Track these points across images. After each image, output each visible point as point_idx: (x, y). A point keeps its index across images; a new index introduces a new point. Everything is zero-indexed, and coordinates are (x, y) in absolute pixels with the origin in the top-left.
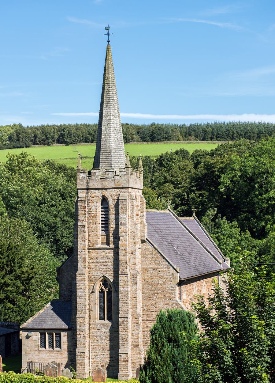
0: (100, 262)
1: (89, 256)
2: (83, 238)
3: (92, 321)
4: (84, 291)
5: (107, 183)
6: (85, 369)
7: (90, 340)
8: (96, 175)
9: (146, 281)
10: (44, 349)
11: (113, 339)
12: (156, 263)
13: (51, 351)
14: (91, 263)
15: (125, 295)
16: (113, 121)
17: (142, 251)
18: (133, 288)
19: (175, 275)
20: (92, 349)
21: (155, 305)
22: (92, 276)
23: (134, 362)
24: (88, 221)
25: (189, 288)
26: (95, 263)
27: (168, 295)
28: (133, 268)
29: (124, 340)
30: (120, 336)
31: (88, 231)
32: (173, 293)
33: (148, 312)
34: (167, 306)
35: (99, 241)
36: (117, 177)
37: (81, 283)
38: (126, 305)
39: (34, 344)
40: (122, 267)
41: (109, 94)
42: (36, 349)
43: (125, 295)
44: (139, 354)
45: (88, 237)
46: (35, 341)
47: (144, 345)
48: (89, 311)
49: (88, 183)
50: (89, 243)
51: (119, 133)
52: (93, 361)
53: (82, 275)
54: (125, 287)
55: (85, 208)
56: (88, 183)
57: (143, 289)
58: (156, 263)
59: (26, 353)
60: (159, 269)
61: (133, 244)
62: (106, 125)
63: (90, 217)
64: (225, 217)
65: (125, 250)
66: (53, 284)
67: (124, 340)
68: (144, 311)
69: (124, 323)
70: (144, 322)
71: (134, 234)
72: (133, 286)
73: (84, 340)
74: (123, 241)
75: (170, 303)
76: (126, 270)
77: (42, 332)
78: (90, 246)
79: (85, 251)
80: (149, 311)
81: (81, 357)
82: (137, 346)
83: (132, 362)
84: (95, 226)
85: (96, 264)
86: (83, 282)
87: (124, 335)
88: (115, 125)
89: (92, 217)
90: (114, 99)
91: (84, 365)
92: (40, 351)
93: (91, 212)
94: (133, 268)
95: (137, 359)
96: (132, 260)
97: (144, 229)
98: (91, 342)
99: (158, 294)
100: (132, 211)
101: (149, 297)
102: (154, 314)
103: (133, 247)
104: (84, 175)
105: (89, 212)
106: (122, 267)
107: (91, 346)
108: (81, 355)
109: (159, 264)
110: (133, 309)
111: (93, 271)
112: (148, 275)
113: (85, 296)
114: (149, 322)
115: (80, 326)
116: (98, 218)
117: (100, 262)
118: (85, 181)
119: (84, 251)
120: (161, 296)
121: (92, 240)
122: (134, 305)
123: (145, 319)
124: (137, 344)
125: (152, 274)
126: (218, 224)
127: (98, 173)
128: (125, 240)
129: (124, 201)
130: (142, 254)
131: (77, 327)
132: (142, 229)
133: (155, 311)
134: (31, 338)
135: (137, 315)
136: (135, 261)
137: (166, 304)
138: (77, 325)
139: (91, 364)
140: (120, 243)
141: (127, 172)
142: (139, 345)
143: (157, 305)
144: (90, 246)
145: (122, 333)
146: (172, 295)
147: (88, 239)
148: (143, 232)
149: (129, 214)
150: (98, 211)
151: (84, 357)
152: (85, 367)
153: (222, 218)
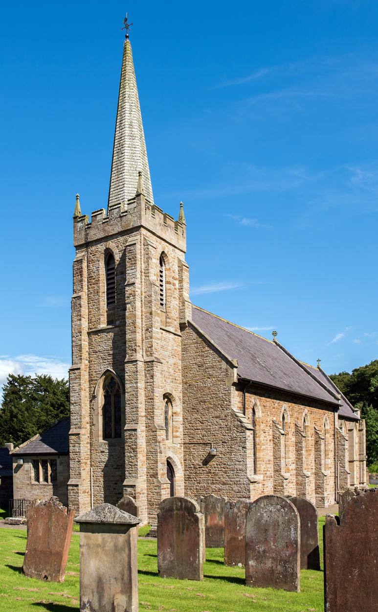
0: (104, 351)
1: (90, 344)
2: (78, 316)
3: (94, 440)
4: (79, 394)
5: (111, 228)
6: (79, 510)
7: (92, 468)
8: (97, 219)
9: (188, 385)
10: (37, 483)
11: (121, 466)
12: (202, 356)
13: (45, 485)
14: (92, 353)
15: (133, 395)
16: (128, 143)
17: (182, 341)
18: (148, 384)
19: (229, 371)
20: (94, 481)
21: (201, 420)
22: (94, 373)
23: (150, 501)
24: (89, 291)
25: (268, 404)
26: (97, 352)
27: (219, 402)
28: (148, 353)
29: (131, 465)
30: (126, 458)
31: (88, 307)
32: (227, 399)
33: (191, 431)
34: (217, 420)
35: (102, 319)
36: (124, 214)
37: (76, 383)
38: (134, 410)
39: (25, 476)
40: (129, 352)
41: (124, 107)
42: (28, 482)
43: (133, 395)
44: (157, 488)
45: (88, 315)
46: (27, 471)
47: (186, 479)
48: (91, 426)
49: (87, 235)
50: (90, 324)
51: (139, 161)
52: (95, 499)
53: (76, 371)
54: (134, 381)
55: (81, 272)
56: (87, 235)
57: (183, 397)
58: (202, 356)
59: (17, 488)
60: (207, 365)
61: (148, 315)
62: (119, 151)
63: (91, 285)
64: (371, 406)
65: (134, 323)
66: (219, 470)
67: (131, 465)
68: (185, 429)
69: (131, 439)
70: (185, 446)
71: (149, 299)
72: (148, 381)
73: (79, 467)
74: (131, 310)
75: (223, 416)
76: (134, 354)
77: (35, 458)
78: (91, 329)
79: (81, 335)
80: (192, 430)
81: (73, 493)
82: (155, 475)
83: (148, 501)
84: (97, 297)
85: (98, 354)
86: (77, 381)
87: (131, 457)
88: (133, 149)
89: (94, 284)
90: (133, 113)
91: (78, 505)
92: (33, 485)
93: (92, 276)
94: (148, 353)
95: (156, 496)
96: (147, 341)
97: (183, 308)
98: (93, 472)
99: (205, 402)
100: (146, 264)
101: (193, 409)
102: (199, 433)
103: (148, 320)
104: (82, 224)
105: (89, 277)
106: (129, 352)
107: (93, 476)
108: (74, 490)
109: (207, 357)
110: (149, 418)
111: (95, 365)
112: (191, 375)
113: (80, 402)
114: (193, 445)
115: (74, 446)
116: (100, 285)
117: (104, 351)
118: (83, 233)
119: (79, 334)
120: (210, 406)
121: (94, 319)
122: (149, 410)
123: (187, 441)
124: (154, 472)
125: (197, 373)
126: (365, 411)
127: (99, 216)
128: (134, 308)
129: (132, 248)
130: (182, 345)
131: (70, 448)
132: (181, 308)
133: (200, 428)
134: (22, 467)
135: (154, 426)
136: (152, 342)
137: (217, 417)
138: (71, 445)
139: (94, 503)
140: (127, 314)
141: (138, 202)
142: (157, 474)
143: (204, 419)
144: (91, 329)
145: (129, 455)
146: (225, 402)
147: (88, 318)
148: (182, 312)
149: (141, 268)
150: (100, 273)
151: (78, 493)
152: (79, 507)
153: (369, 406)
